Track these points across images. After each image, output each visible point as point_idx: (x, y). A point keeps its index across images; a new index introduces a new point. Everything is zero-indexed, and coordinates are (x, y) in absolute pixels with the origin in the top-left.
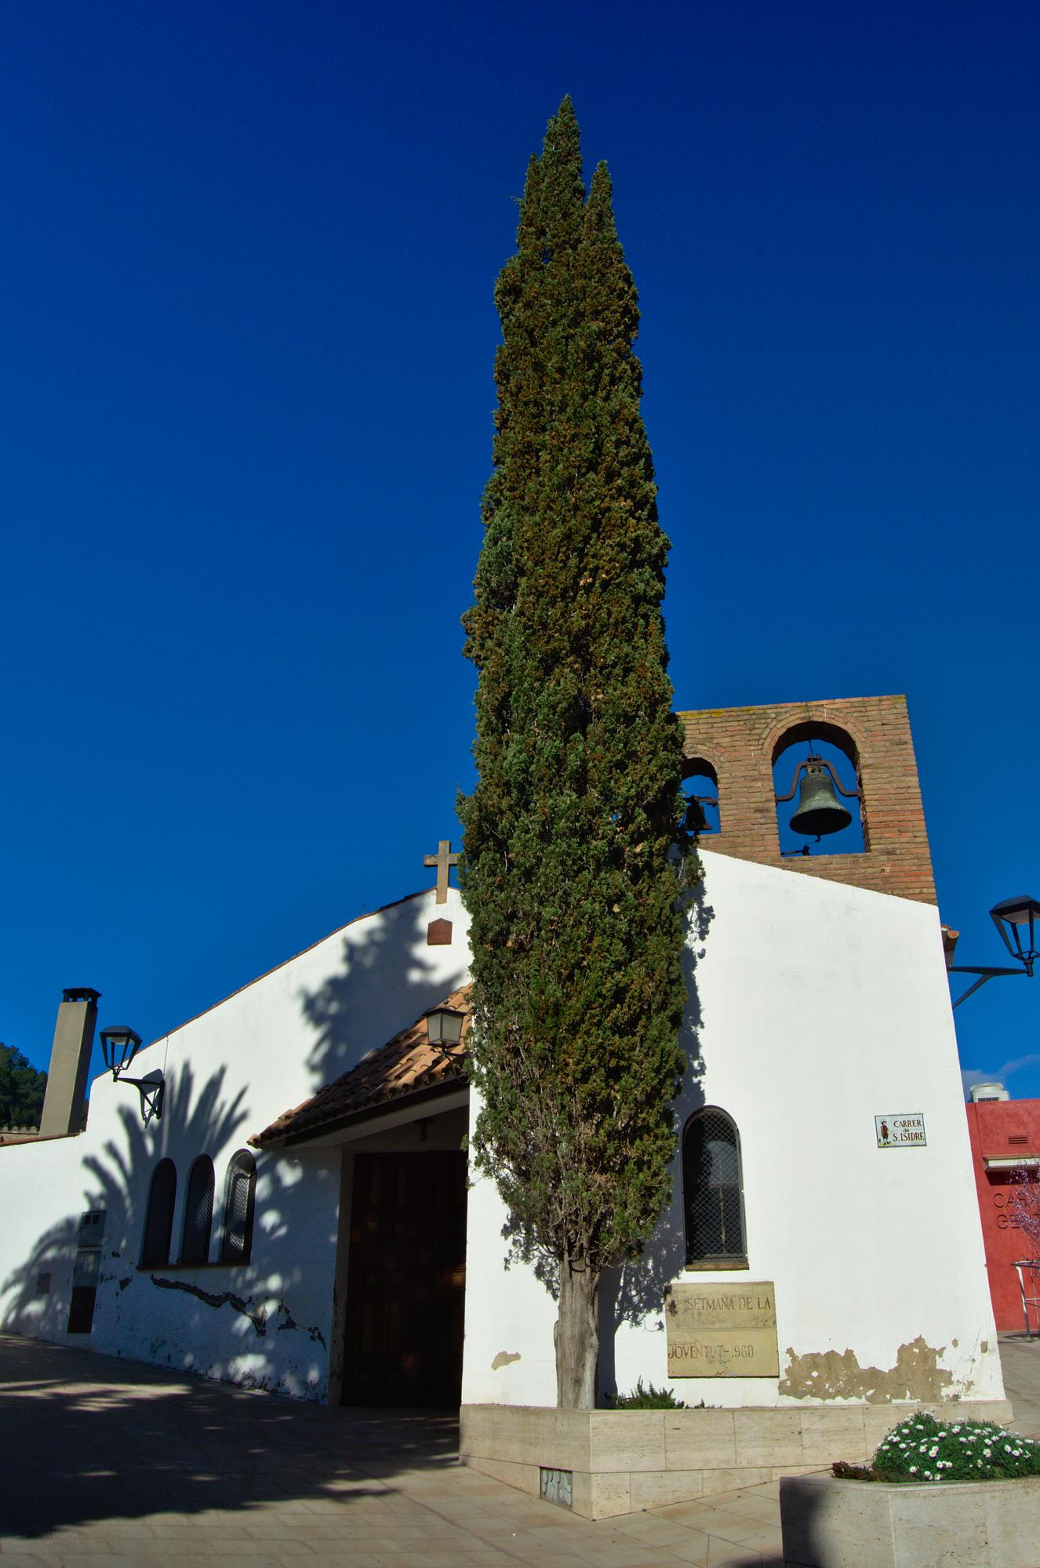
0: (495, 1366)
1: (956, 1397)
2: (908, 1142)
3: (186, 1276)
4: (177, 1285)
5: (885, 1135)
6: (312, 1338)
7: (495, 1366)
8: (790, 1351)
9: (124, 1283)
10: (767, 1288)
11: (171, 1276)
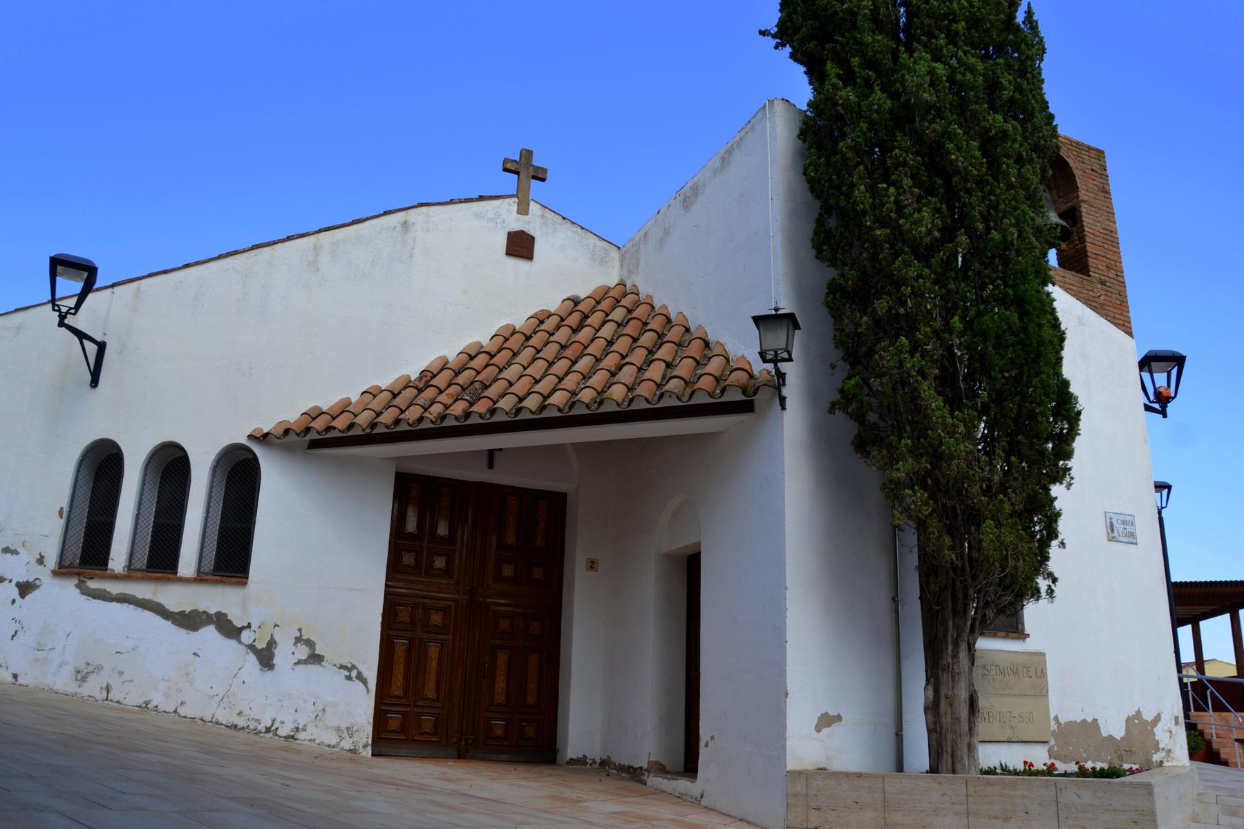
0: (818, 729)
1: (1162, 762)
2: (1126, 539)
3: (143, 590)
4: (122, 599)
5: (1112, 530)
6: (349, 678)
7: (818, 729)
8: (1056, 718)
9: (25, 589)
10: (647, 741)
11: (114, 588)
